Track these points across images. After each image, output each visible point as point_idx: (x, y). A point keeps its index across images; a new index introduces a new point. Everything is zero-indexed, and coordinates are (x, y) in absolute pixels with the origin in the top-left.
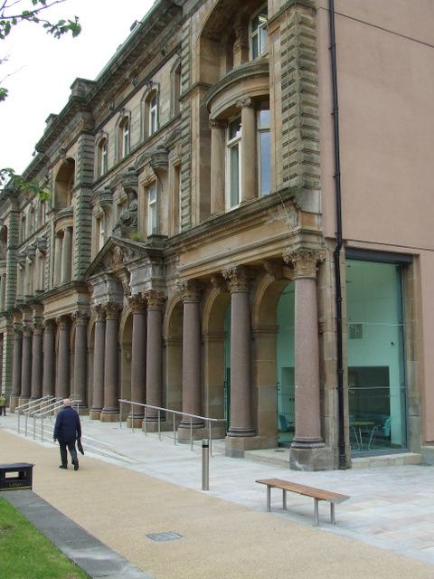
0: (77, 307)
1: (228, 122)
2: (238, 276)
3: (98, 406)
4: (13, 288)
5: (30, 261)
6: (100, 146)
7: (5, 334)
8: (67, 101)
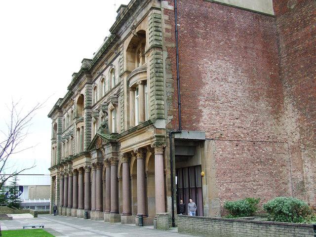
0: (111, 154)
1: (134, 88)
2: (139, 152)
3: (108, 211)
4: (60, 154)
5: (67, 141)
6: (95, 89)
7: (57, 176)
8: (114, 20)
